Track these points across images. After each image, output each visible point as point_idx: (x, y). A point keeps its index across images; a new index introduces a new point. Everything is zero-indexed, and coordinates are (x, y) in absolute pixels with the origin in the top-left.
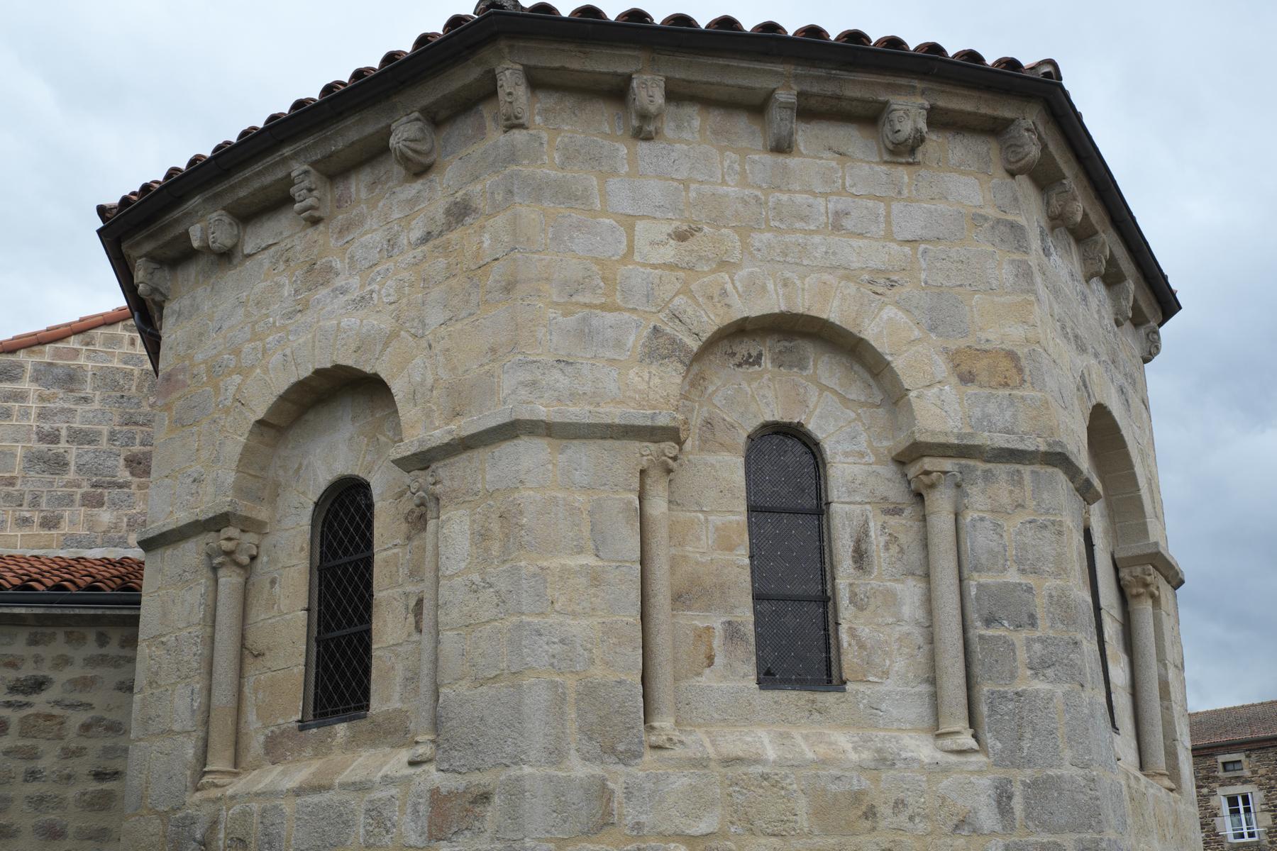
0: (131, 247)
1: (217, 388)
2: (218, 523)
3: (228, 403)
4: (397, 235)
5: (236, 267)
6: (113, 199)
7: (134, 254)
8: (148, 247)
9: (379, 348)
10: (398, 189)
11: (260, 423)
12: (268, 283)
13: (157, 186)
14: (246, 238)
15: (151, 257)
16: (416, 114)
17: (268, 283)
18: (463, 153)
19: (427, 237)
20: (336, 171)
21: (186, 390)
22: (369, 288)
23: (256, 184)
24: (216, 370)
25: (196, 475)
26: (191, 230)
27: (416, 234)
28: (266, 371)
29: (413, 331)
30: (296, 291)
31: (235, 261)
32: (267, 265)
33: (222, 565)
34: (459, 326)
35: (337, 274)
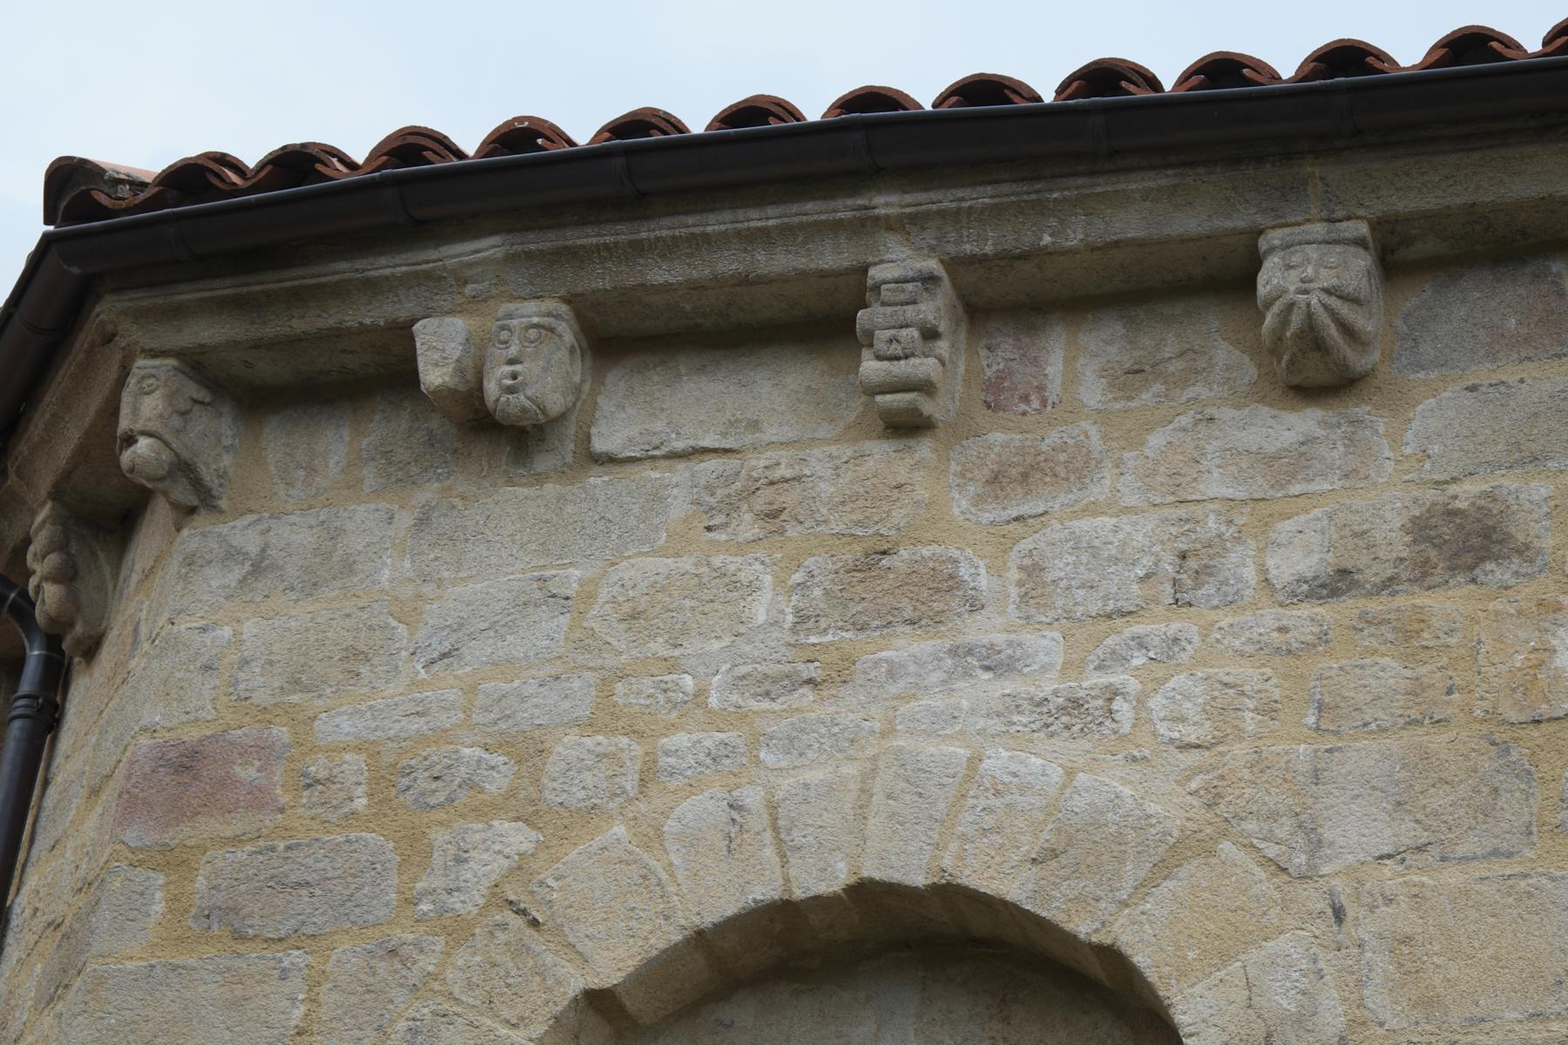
0: (140, 316)
1: (415, 851)
3: (467, 904)
4: (1217, 545)
5: (540, 479)
6: (141, 148)
7: (133, 334)
8: (206, 332)
9: (1132, 872)
10: (1227, 413)
11: (598, 1001)
12: (687, 564)
13: (344, 176)
14: (605, 404)
15: (196, 364)
16: (1363, 229)
17: (687, 564)
18: (1482, 374)
19: (1337, 583)
20: (1006, 303)
22: (1103, 679)
23: (728, 264)
24: (407, 790)
27: (1298, 557)
28: (654, 837)
29: (1272, 851)
30: (802, 618)
31: (543, 463)
32: (678, 506)
34: (1453, 877)
35: (975, 607)
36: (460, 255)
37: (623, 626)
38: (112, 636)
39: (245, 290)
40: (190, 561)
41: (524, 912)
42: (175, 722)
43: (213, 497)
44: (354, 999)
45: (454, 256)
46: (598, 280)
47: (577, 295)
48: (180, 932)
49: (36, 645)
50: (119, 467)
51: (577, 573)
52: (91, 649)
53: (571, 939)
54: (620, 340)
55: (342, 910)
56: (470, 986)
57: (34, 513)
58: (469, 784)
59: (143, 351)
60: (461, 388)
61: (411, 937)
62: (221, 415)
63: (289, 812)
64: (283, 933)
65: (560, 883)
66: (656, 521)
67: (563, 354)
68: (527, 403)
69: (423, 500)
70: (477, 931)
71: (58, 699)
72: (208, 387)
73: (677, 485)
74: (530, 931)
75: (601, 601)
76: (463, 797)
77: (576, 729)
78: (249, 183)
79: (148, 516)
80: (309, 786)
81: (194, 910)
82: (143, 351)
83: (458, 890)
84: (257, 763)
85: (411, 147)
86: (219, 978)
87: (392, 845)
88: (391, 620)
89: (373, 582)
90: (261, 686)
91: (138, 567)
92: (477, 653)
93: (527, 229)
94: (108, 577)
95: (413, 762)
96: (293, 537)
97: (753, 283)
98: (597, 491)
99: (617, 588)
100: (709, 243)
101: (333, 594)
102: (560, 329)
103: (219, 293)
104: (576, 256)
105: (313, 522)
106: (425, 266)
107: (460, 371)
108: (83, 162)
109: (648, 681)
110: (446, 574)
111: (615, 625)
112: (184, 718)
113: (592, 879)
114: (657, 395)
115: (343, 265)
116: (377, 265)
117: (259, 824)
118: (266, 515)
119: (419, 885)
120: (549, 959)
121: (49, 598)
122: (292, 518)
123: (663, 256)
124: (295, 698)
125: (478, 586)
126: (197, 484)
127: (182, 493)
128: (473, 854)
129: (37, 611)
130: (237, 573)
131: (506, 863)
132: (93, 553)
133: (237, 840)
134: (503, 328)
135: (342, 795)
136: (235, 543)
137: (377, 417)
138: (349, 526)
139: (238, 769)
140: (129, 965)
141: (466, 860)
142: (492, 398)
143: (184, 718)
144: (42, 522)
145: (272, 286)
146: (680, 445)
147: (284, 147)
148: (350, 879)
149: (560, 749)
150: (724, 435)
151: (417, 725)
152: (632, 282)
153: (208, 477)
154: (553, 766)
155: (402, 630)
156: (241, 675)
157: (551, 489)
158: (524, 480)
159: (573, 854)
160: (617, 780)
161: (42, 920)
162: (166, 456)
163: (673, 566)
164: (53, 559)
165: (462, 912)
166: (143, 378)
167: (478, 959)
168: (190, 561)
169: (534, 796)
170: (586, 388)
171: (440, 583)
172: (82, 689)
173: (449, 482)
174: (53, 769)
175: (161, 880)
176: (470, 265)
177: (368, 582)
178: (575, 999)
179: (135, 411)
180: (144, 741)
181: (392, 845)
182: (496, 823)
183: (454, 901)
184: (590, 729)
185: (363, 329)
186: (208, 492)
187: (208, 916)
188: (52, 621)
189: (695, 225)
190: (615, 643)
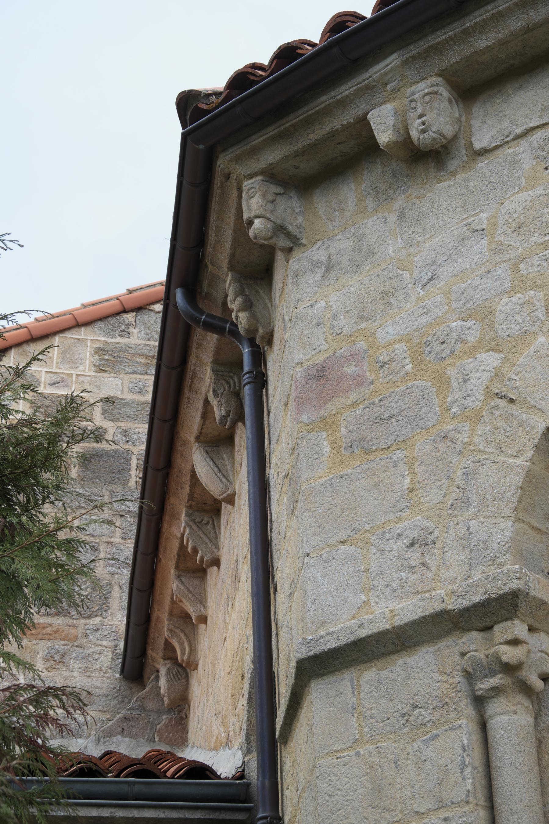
0: (238, 159)
1: (442, 383)
2: (499, 608)
5: (453, 174)
6: (214, 78)
7: (239, 170)
8: (271, 156)
12: (539, 191)
13: (310, 50)
15: (271, 175)
17: (539, 191)
21: (367, 390)
25: (414, 534)
26: (373, 117)
31: (453, 165)
32: (527, 162)
33: (497, 691)
36: (379, 71)
37: (515, 234)
38: (276, 329)
39: (282, 128)
40: (296, 275)
41: (504, 397)
42: (310, 355)
43: (298, 239)
44: (432, 467)
45: (376, 73)
46: (452, 58)
47: (444, 70)
48: (340, 458)
49: (245, 346)
50: (249, 238)
51: (484, 215)
52: (270, 341)
53: (533, 403)
54: (473, 87)
55: (414, 424)
56: (488, 443)
57: (225, 282)
58: (460, 340)
59: (245, 177)
60: (399, 139)
61: (452, 426)
62: (291, 197)
63: (376, 383)
64: (389, 444)
65: (519, 376)
66: (518, 174)
67: (446, 104)
68: (434, 135)
69: (399, 206)
70: (484, 414)
71: (264, 371)
72: (281, 185)
73: (524, 152)
74: (512, 405)
75: (500, 225)
76: (458, 348)
77: (506, 295)
78: (268, 72)
79: (275, 264)
80: (382, 367)
81: (344, 445)
82: (245, 177)
83: (469, 396)
84: (354, 363)
85: (340, 24)
86: (365, 475)
87: (430, 383)
88: (399, 271)
89: (385, 255)
90: (345, 324)
91: (278, 291)
92: (445, 273)
93: (408, 45)
94: (267, 301)
95: (428, 339)
96: (341, 246)
97: (533, 30)
98: (484, 170)
99: (507, 215)
100: (503, 16)
101: (368, 268)
102: (440, 91)
103: (271, 134)
104: (437, 49)
105: (349, 235)
106: (364, 83)
107: (396, 131)
108: (190, 91)
109: (536, 258)
110: (420, 239)
111: (511, 235)
112: (314, 352)
113: (534, 369)
114: (501, 109)
115: (324, 98)
116: (341, 91)
117: (363, 393)
118: (326, 240)
119: (449, 400)
120: (524, 417)
121: (242, 319)
122: (338, 237)
123: (481, 33)
124: (363, 325)
125: (437, 239)
126: (289, 235)
127: (282, 242)
128: (471, 375)
129: (240, 328)
130: (319, 273)
131: (489, 375)
132: (257, 292)
133: (355, 404)
134: (411, 101)
135: (399, 366)
136: (315, 259)
137: (365, 172)
138: (367, 231)
139: (346, 369)
140: (321, 481)
141: (469, 380)
142: (416, 139)
143: (314, 352)
144: (229, 286)
145: (294, 121)
146: (519, 131)
147: (280, 48)
148: (414, 407)
149: (500, 307)
150: (541, 117)
151: (426, 319)
152: (469, 52)
153: (293, 229)
154: (499, 318)
155: (406, 274)
156: (335, 323)
157: (460, 177)
158: (445, 178)
159: (521, 360)
160: (534, 314)
161: (281, 476)
162: (269, 225)
163: (533, 194)
164: (239, 300)
165: (474, 406)
166: (249, 190)
167: (488, 428)
168: (296, 275)
169: (493, 336)
170: (464, 119)
171: (418, 244)
172: (271, 361)
173: (409, 193)
174: (270, 404)
175: (325, 435)
176: (386, 74)
177: (383, 256)
178: (544, 434)
179: (249, 208)
180: (299, 369)
181: (430, 383)
182: (478, 356)
183: (468, 402)
184: (512, 292)
185: (345, 128)
186: (295, 237)
187: (351, 446)
188: (248, 331)
189: (493, 9)
190: (513, 244)
